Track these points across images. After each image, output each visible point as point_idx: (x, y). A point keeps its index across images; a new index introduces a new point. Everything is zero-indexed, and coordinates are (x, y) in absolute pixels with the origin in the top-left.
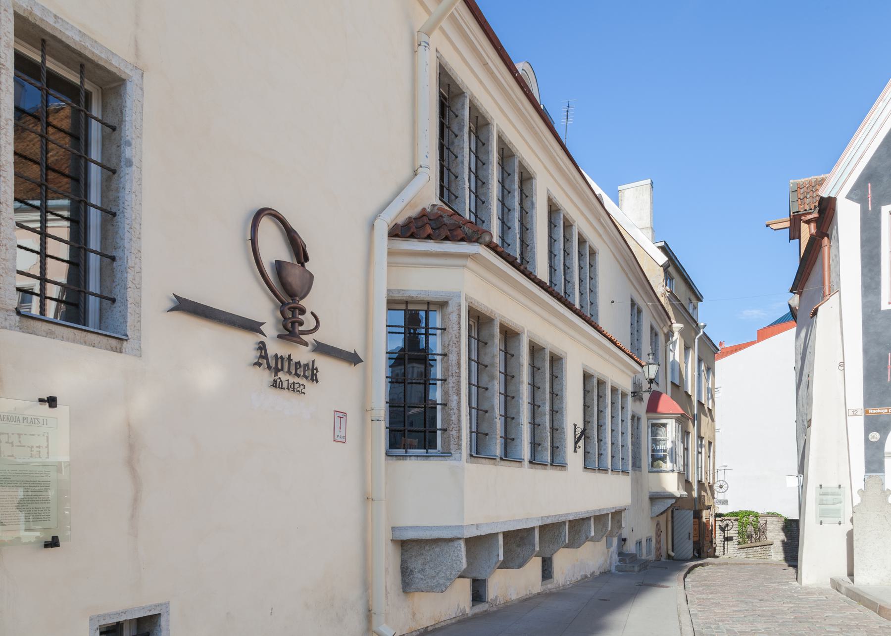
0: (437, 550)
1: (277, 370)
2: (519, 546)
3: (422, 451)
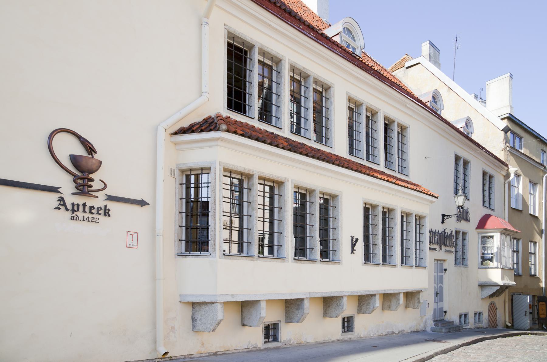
0: (207, 308)
1: (73, 211)
2: (297, 310)
3: (198, 253)
